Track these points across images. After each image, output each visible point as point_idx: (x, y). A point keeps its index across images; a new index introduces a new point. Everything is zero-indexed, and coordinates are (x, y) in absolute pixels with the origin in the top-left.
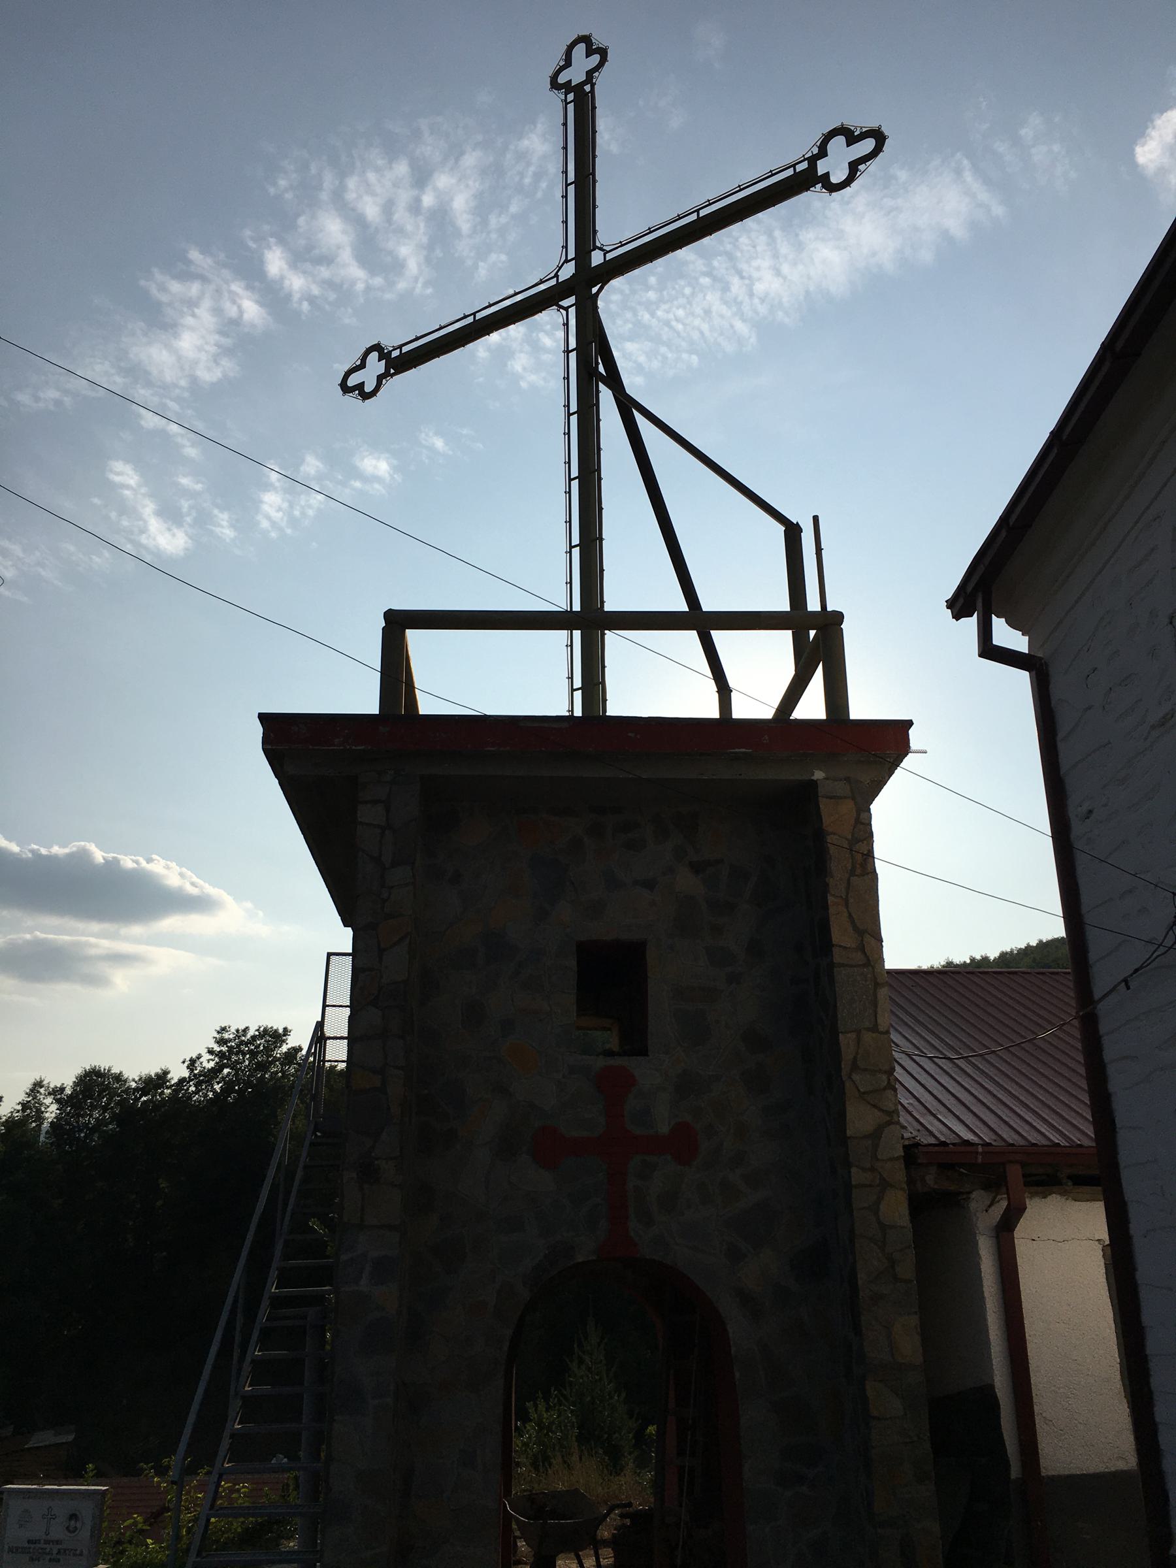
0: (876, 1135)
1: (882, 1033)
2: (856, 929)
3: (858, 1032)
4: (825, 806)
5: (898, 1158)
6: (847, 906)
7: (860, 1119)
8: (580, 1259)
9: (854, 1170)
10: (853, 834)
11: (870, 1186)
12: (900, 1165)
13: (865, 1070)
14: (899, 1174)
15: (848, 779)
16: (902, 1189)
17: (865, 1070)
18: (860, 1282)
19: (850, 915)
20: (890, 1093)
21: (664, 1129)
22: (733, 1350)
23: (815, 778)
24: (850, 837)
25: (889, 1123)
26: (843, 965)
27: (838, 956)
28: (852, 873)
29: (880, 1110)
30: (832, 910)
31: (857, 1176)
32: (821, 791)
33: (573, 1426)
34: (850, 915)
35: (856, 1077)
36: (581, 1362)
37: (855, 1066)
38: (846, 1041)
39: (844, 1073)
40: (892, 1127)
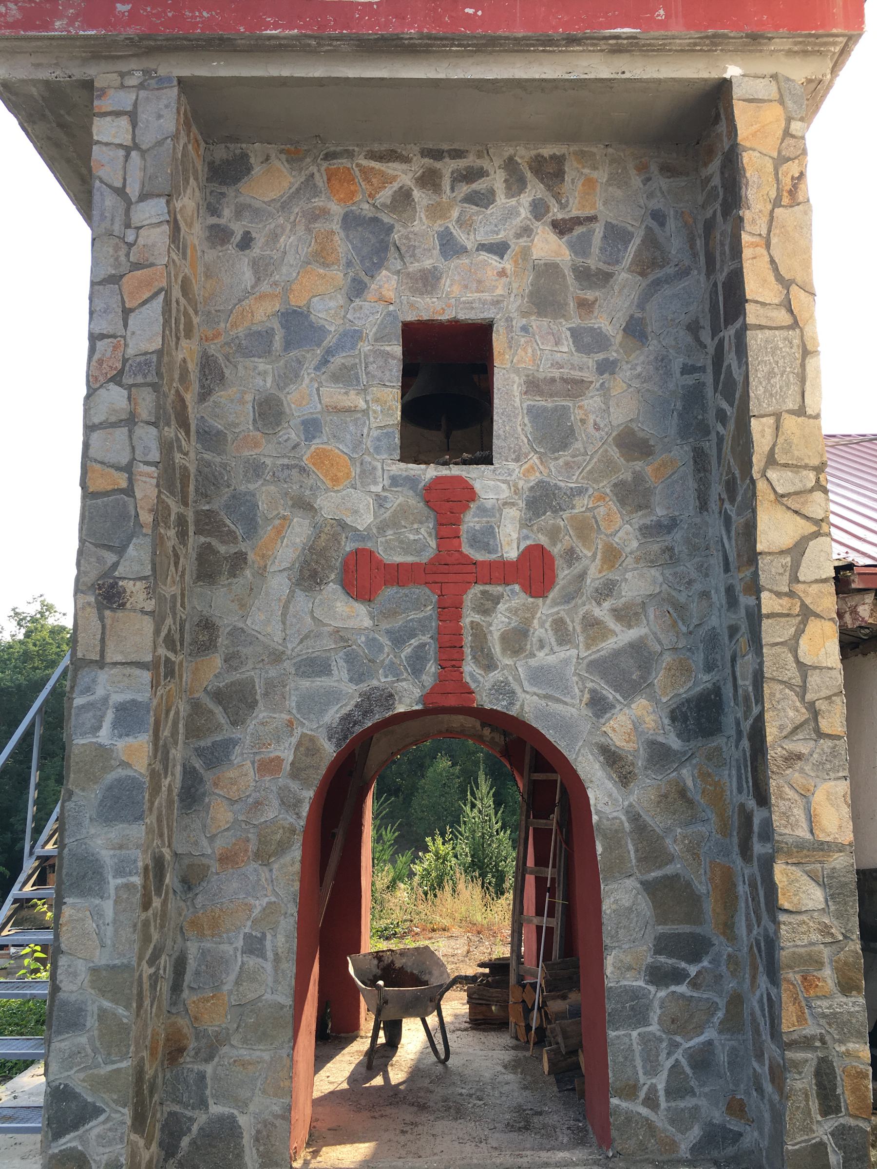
0: (798, 550)
1: (810, 417)
2: (779, 278)
3: (778, 416)
4: (742, 114)
5: (825, 581)
6: (768, 246)
7: (774, 530)
8: (401, 709)
9: (765, 595)
10: (779, 152)
11: (788, 615)
12: (831, 588)
13: (786, 465)
14: (826, 600)
15: (774, 77)
16: (832, 619)
17: (786, 465)
18: (769, 739)
19: (772, 261)
20: (818, 495)
21: (512, 553)
22: (595, 818)
23: (727, 76)
24: (775, 155)
25: (816, 535)
26: (761, 327)
27: (753, 315)
28: (777, 203)
29: (807, 518)
30: (747, 253)
31: (769, 603)
32: (737, 92)
33: (466, 855)
34: (772, 261)
35: (772, 474)
36: (473, 806)
37: (771, 460)
38: (761, 431)
39: (755, 473)
40: (821, 539)
